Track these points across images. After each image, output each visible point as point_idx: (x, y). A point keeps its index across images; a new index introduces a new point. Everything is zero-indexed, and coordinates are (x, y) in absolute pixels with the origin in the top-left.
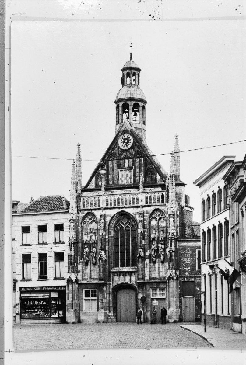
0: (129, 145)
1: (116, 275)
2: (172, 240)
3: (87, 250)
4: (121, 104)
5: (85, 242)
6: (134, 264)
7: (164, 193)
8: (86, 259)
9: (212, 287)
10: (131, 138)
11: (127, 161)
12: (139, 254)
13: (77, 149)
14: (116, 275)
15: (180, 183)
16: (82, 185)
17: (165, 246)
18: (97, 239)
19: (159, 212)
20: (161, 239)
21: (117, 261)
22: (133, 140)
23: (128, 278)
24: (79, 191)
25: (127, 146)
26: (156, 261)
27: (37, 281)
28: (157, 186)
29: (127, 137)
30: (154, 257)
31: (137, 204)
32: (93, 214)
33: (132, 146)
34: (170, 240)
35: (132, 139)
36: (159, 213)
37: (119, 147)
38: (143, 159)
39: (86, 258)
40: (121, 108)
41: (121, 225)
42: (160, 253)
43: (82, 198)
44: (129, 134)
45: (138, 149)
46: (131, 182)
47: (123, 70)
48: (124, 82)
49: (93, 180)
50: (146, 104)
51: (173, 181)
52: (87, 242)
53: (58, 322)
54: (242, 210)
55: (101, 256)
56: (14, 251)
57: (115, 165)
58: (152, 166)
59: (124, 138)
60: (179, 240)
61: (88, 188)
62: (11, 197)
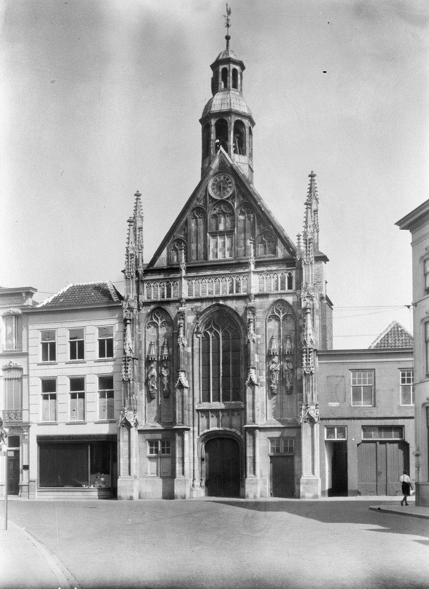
0: (228, 192)
9: (195, 464)
18: (171, 353)
25: (224, 194)
27: (95, 425)
29: (224, 178)
31: (281, 289)
35: (234, 182)
45: (244, 198)
48: (217, 87)
49: (164, 253)
52: (291, 352)
57: (201, 228)
62: (426, 284)
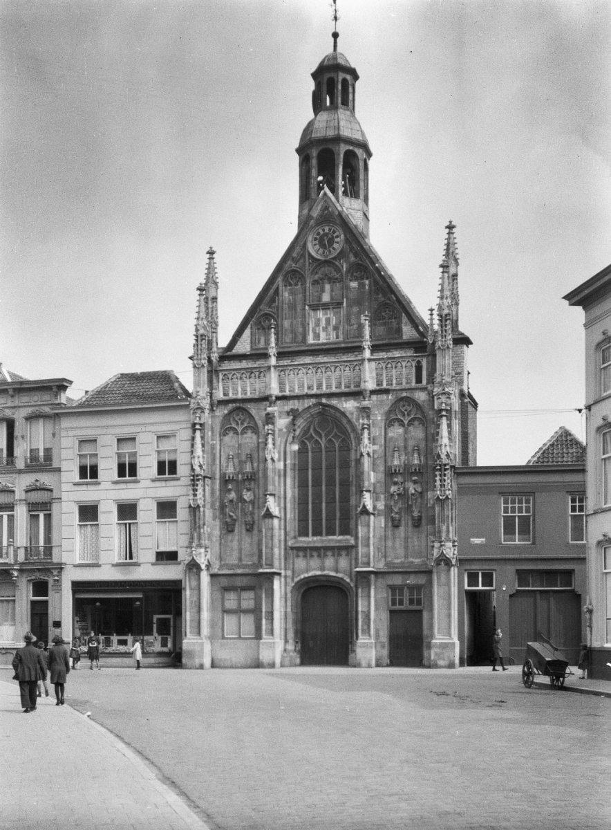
2: (446, 470)
3: (233, 495)
4: (314, 153)
5: (229, 477)
6: (345, 531)
11: (328, 287)
13: (207, 261)
17: (422, 487)
19: (409, 405)
22: (345, 236)
24: (215, 357)
32: (245, 410)
34: (440, 470)
36: (242, 418)
37: (310, 255)
38: (367, 282)
39: (231, 514)
40: (314, 162)
41: (314, 438)
42: (410, 503)
43: (220, 374)
46: (337, 337)
49: (247, 333)
50: (371, 158)
51: (446, 331)
53: (161, 665)
55: (268, 510)
56: (136, 665)
60: (461, 473)
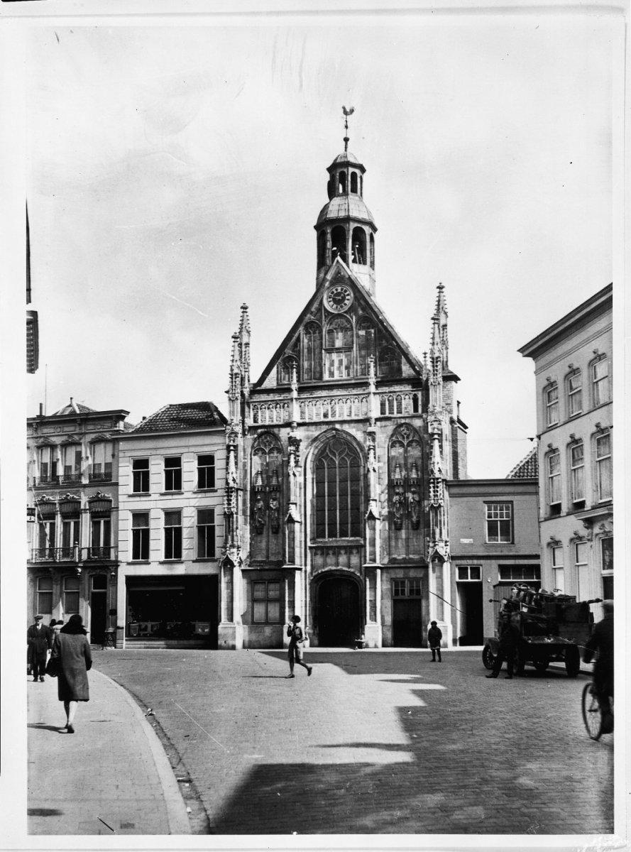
1: (331, 552)
3: (261, 504)
7: (419, 395)
8: (259, 522)
10: (350, 291)
12: (368, 512)
14: (319, 552)
15: (449, 374)
16: (251, 382)
20: (414, 482)
21: (333, 526)
23: (343, 559)
26: (401, 524)
28: (401, 381)
30: (398, 518)
33: (352, 306)
38: (373, 331)
44: (347, 284)
47: (329, 170)
54: (236, 468)
58: (391, 344)
59: (335, 292)
61: (263, 387)
